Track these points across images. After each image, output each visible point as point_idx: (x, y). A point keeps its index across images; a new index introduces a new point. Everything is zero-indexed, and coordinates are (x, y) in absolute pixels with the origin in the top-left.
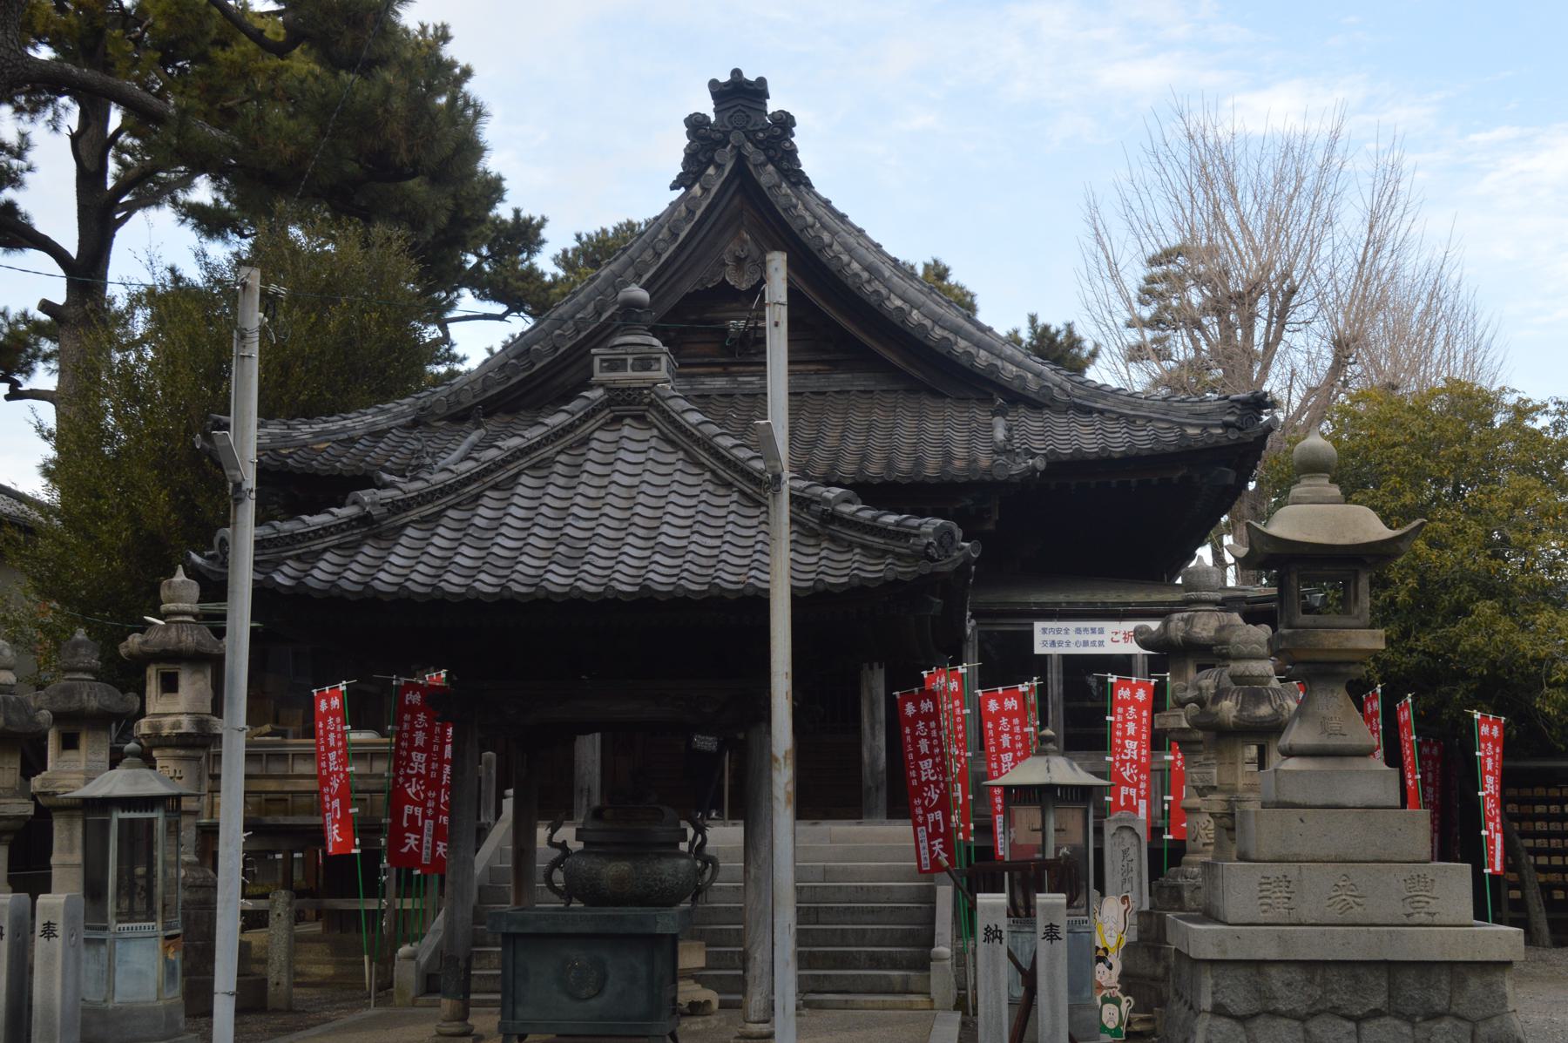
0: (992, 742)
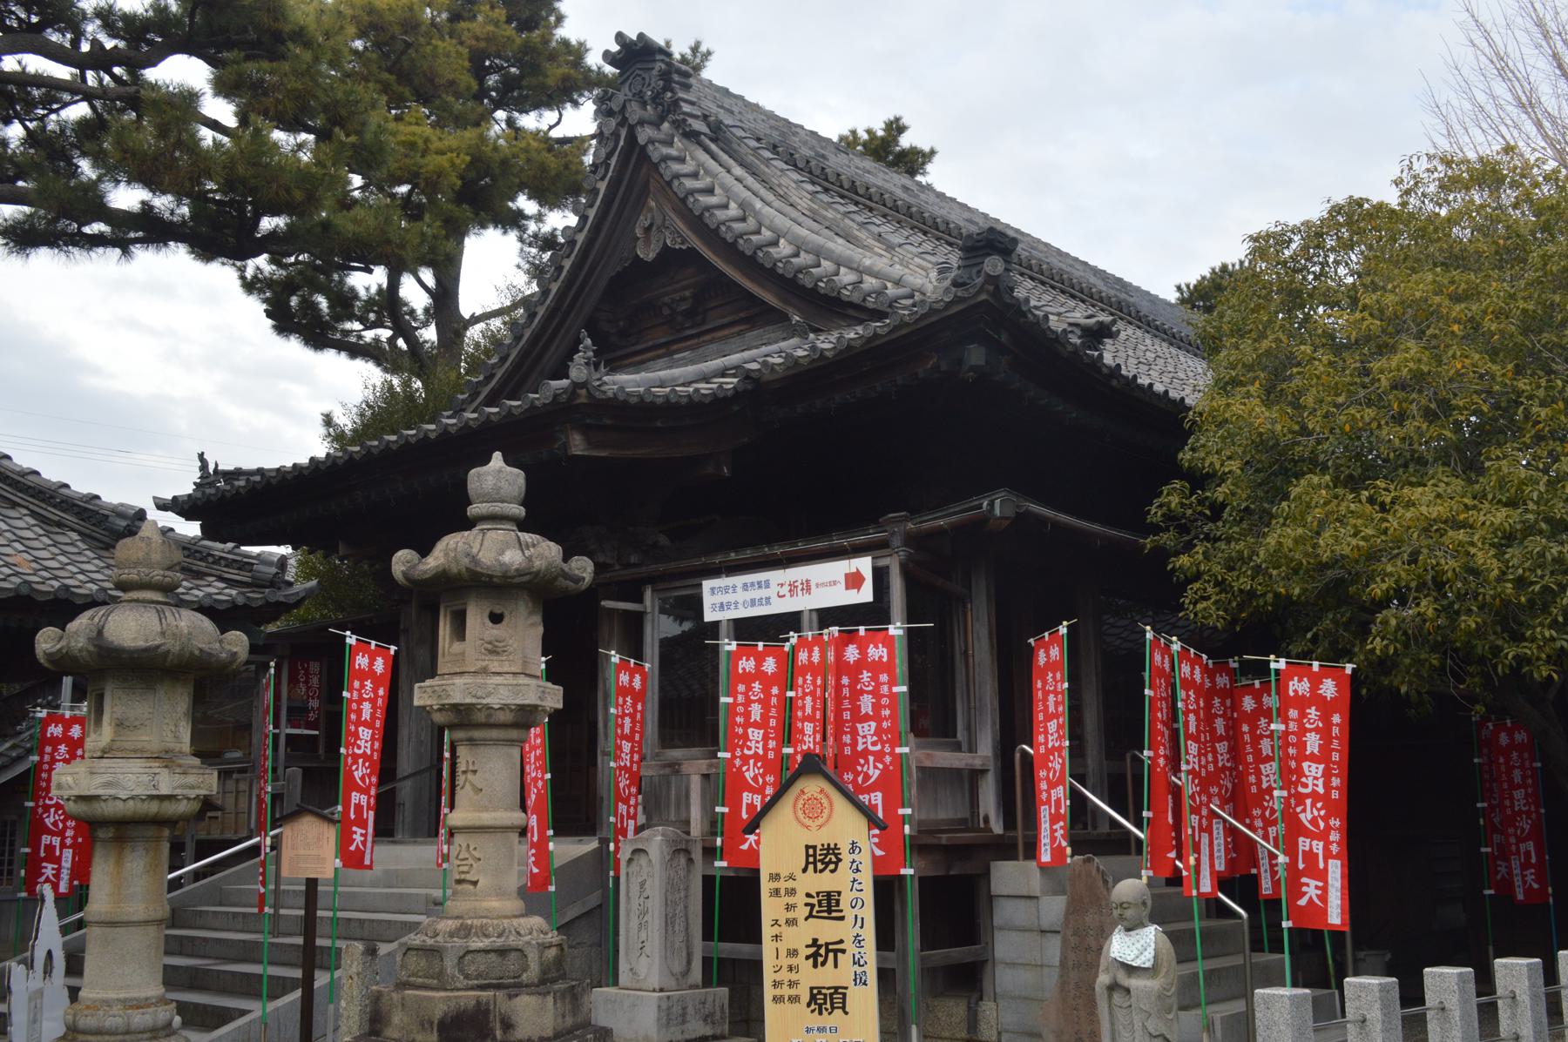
0: (1249, 749)
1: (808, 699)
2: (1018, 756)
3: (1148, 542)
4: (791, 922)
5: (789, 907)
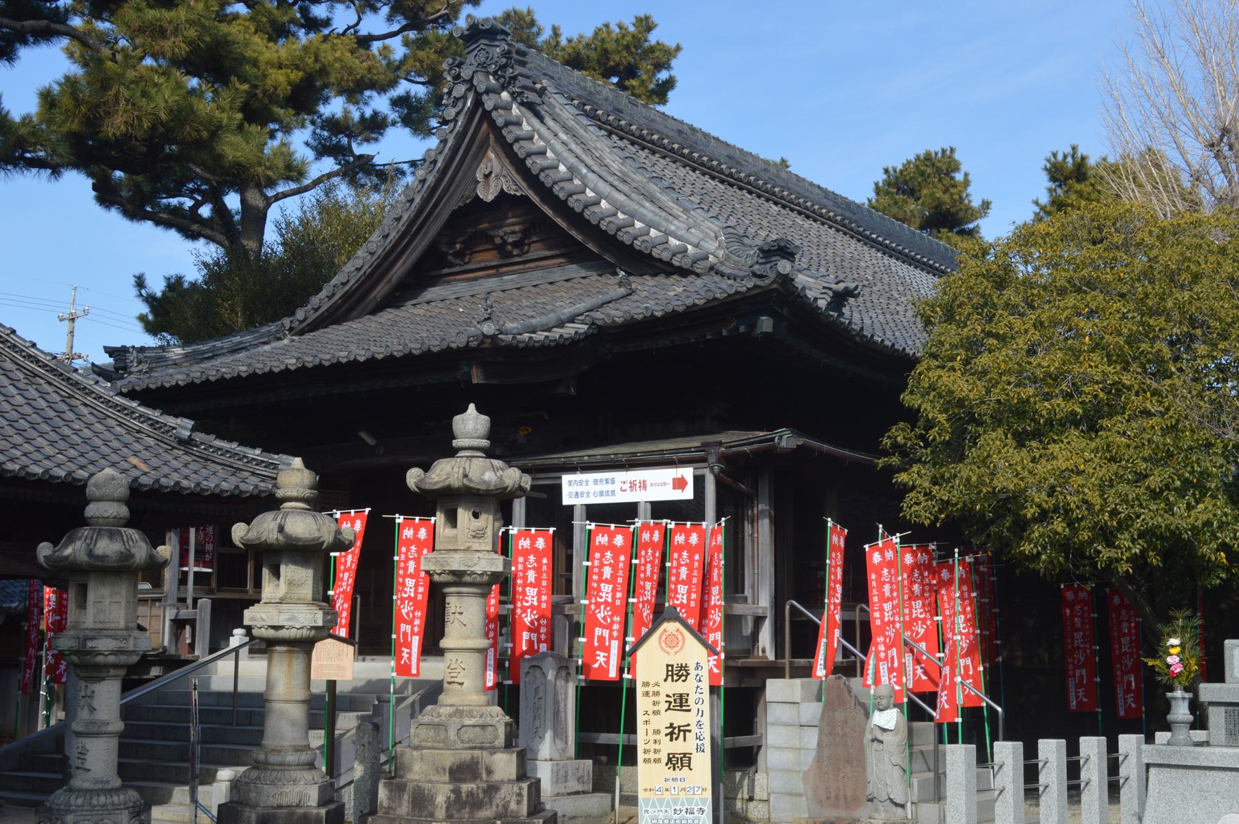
0: (875, 592)
1: (649, 566)
2: (788, 607)
3: (881, 462)
4: (656, 713)
5: (655, 703)
